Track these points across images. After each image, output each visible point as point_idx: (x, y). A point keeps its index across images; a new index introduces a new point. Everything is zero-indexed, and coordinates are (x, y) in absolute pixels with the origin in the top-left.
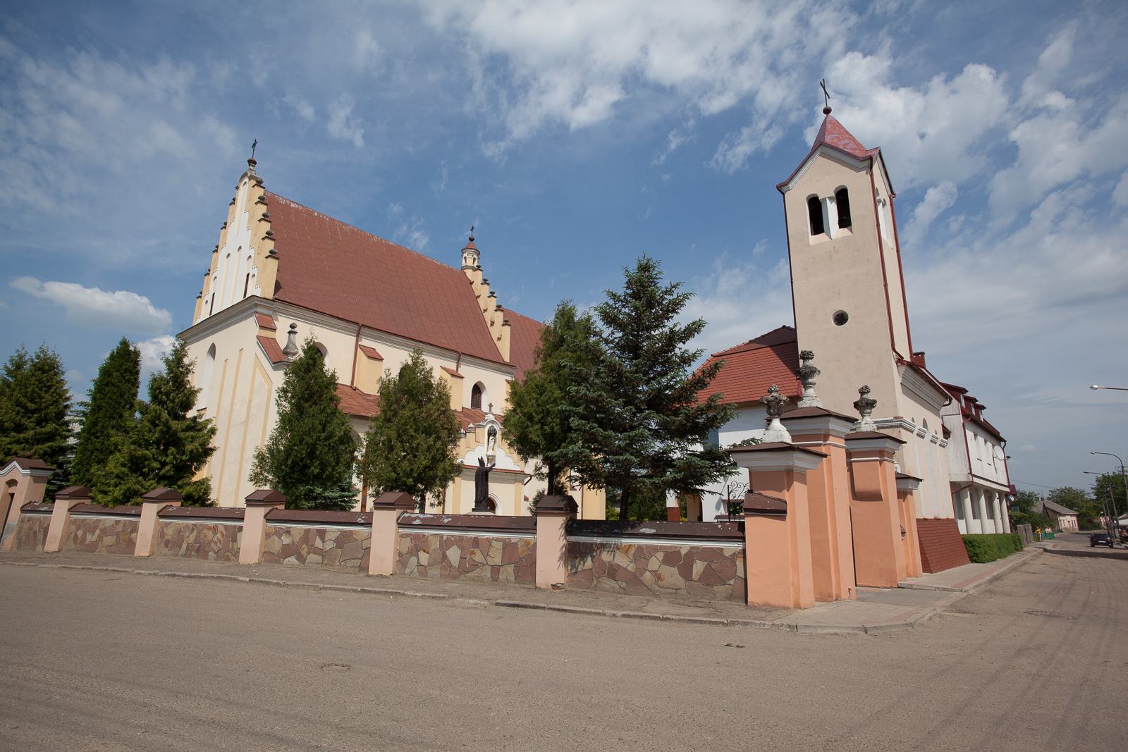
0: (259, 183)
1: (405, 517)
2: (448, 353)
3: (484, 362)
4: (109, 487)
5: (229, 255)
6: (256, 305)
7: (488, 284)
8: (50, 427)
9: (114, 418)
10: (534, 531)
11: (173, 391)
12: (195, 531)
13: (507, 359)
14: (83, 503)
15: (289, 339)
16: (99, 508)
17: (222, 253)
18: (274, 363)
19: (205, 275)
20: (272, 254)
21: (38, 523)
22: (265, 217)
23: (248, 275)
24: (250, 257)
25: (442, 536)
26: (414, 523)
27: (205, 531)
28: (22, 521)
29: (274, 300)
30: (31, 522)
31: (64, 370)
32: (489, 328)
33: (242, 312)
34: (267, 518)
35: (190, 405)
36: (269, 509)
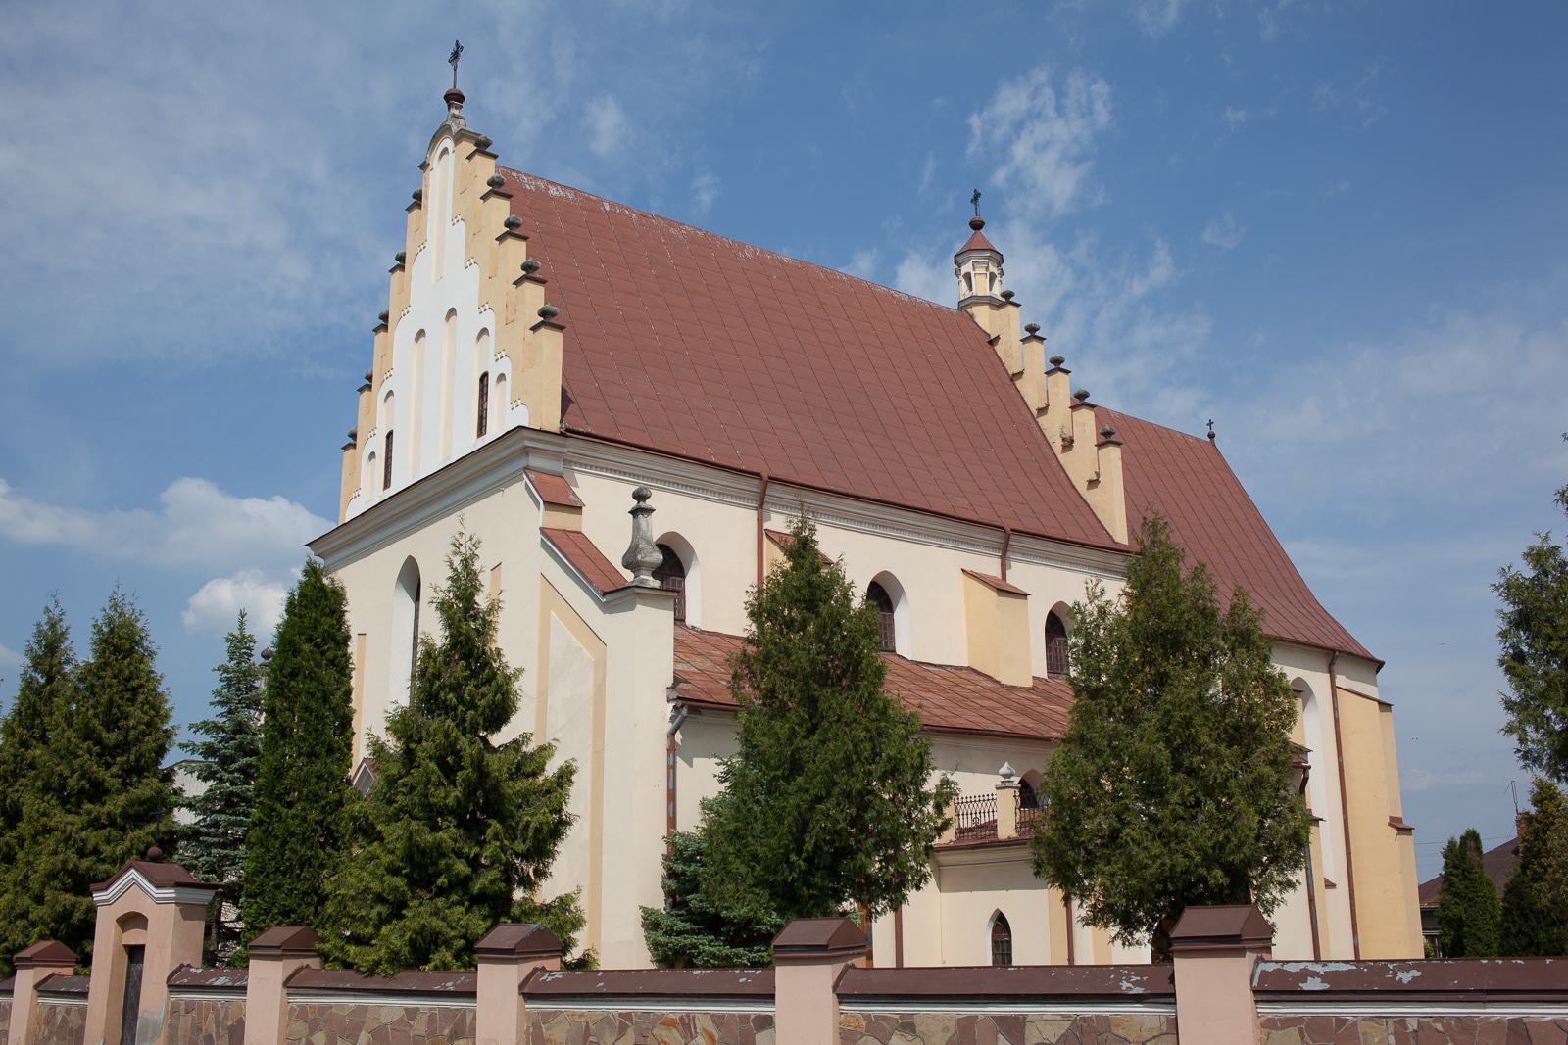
0: (482, 147)
1: (1264, 972)
2: (978, 533)
3: (1067, 550)
4: (367, 926)
5: (422, 333)
6: (526, 451)
7: (1041, 339)
8: (145, 789)
9: (317, 756)
10: (1172, 1000)
11: (466, 678)
12: (630, 1032)
13: (1121, 536)
14: (307, 966)
15: (636, 528)
16: (351, 979)
17: (401, 331)
18: (605, 594)
19: (361, 390)
20: (548, 320)
21: (211, 1016)
22: (512, 229)
23: (484, 377)
24: (484, 331)
25: (1401, 1021)
26: (1306, 987)
27: (660, 1032)
28: (174, 1010)
29: (567, 433)
30: (194, 1014)
31: (153, 648)
32: (1061, 457)
33: (487, 471)
34: (526, 991)
35: (506, 710)
36: (839, 967)
